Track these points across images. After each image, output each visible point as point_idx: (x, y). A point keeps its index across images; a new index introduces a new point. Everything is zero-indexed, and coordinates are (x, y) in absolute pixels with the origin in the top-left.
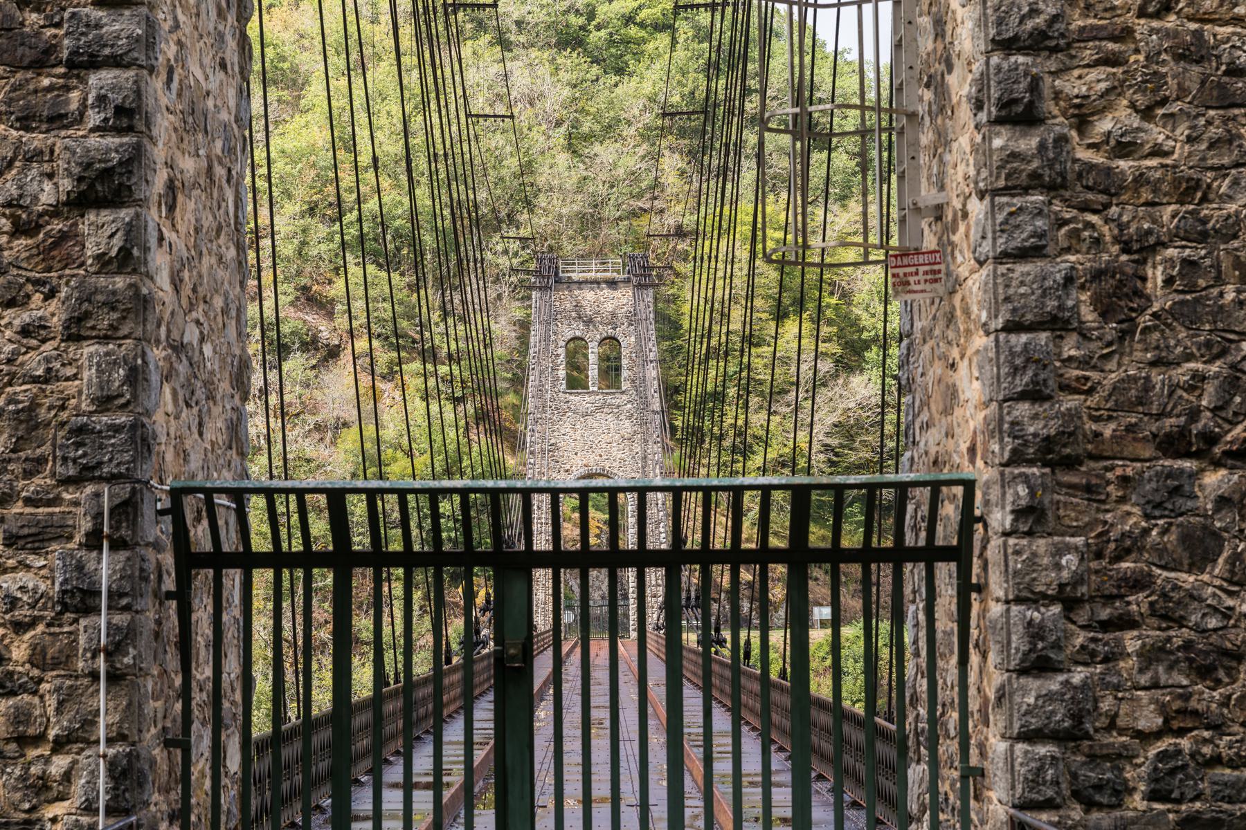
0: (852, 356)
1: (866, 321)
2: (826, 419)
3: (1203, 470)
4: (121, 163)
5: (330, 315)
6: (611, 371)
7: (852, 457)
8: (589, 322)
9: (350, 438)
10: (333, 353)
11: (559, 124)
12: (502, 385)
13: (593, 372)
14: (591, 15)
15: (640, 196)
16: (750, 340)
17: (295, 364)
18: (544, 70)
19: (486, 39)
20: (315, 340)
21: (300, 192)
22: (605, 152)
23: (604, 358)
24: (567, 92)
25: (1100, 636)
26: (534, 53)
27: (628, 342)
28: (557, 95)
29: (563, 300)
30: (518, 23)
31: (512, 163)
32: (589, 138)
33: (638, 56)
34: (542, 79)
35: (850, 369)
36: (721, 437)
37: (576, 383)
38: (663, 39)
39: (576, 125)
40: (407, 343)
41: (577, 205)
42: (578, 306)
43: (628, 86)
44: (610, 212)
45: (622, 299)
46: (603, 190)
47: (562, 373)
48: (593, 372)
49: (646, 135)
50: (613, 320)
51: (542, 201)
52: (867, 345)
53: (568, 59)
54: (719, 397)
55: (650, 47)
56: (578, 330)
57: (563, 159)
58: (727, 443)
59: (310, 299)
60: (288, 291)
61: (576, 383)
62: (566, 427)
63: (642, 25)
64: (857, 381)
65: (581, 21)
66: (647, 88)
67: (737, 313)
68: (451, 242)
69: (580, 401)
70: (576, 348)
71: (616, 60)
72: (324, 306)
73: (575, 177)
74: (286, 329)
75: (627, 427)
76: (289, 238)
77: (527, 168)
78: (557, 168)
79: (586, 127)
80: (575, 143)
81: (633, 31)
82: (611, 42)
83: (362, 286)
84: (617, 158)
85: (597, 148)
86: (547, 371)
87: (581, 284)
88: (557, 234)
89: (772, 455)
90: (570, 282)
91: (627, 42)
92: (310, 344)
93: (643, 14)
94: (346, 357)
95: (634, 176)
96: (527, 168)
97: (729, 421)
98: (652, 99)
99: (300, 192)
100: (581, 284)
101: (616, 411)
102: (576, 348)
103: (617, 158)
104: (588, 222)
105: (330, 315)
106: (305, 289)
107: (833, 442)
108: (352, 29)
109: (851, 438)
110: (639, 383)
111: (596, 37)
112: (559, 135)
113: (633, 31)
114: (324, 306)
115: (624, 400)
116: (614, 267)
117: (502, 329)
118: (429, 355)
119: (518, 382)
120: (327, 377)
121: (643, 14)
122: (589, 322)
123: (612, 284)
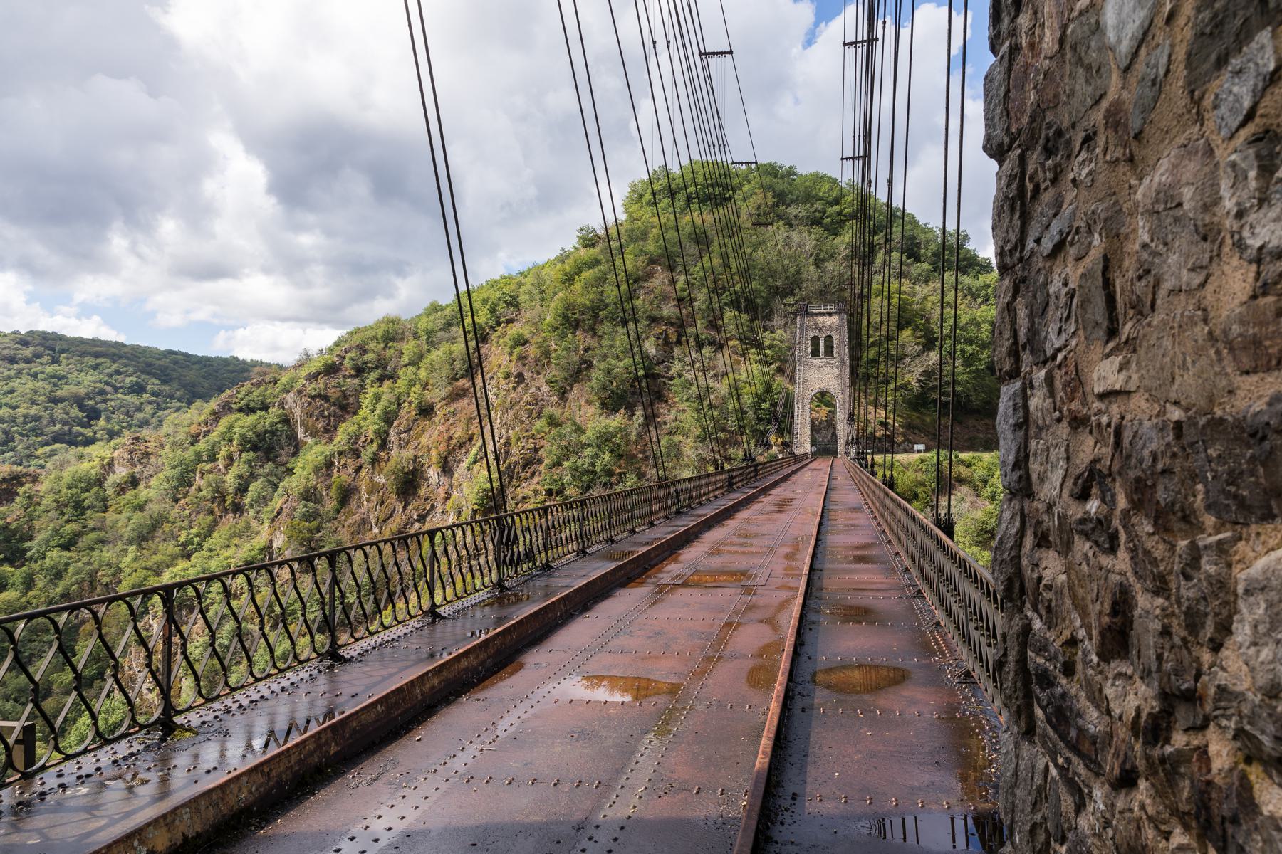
0: (929, 344)
3: (196, 756)
4: (1088, 539)
6: (829, 352)
8: (820, 330)
10: (721, 347)
13: (822, 350)
14: (824, 212)
16: (889, 338)
17: (706, 351)
18: (805, 235)
19: (782, 223)
22: (830, 266)
23: (826, 347)
25: (379, 407)
27: (836, 338)
28: (809, 243)
29: (809, 321)
32: (824, 260)
35: (929, 350)
36: (877, 378)
37: (815, 354)
39: (818, 255)
42: (816, 323)
45: (834, 320)
48: (822, 350)
50: (830, 329)
51: (804, 285)
54: (876, 361)
56: (816, 333)
57: (812, 268)
61: (815, 354)
67: (884, 327)
69: (817, 362)
70: (815, 340)
71: (834, 230)
77: (798, 272)
78: (811, 271)
79: (822, 255)
80: (818, 263)
82: (832, 223)
87: (817, 314)
96: (798, 272)
100: (817, 314)
102: (815, 340)
112: (811, 260)
115: (835, 361)
122: (820, 330)
123: (830, 314)
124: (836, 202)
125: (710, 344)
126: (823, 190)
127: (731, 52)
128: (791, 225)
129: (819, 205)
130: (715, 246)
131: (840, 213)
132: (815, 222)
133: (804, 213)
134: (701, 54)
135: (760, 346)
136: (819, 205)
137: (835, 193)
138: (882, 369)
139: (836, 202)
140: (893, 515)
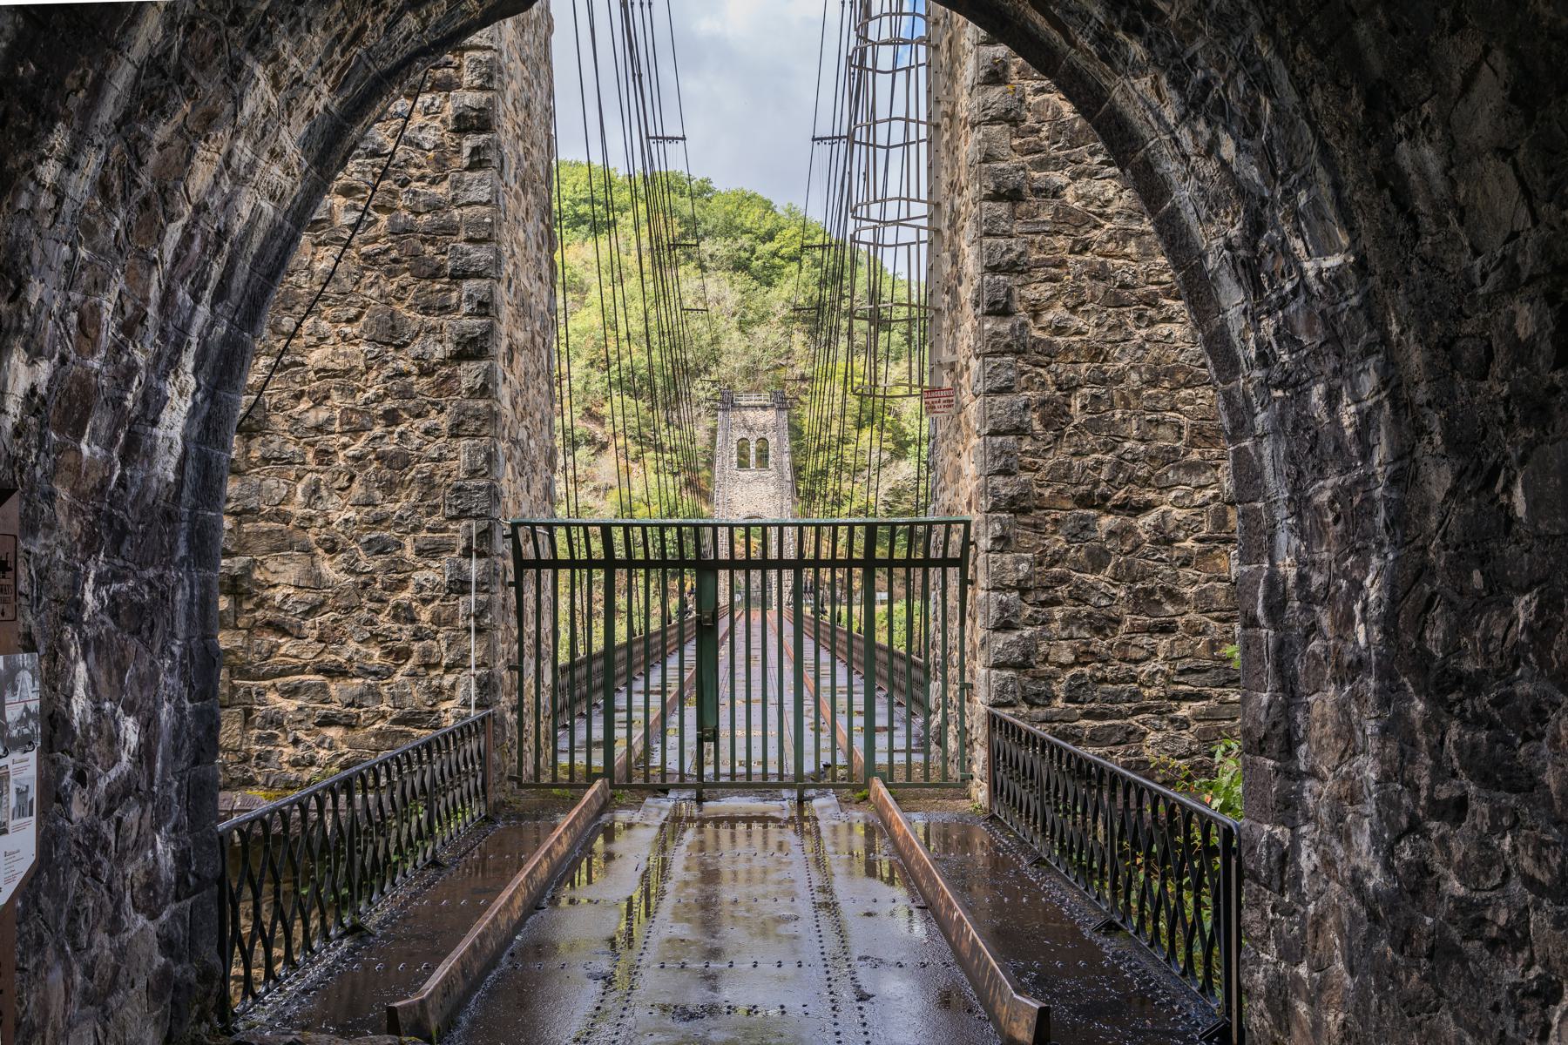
0: (900, 450)
1: (909, 430)
2: (885, 486)
5: (602, 425)
6: (763, 458)
7: (900, 508)
8: (751, 429)
9: (613, 496)
10: (604, 447)
11: (734, 315)
12: (701, 465)
13: (753, 458)
14: (753, 252)
15: (780, 357)
16: (843, 441)
17: (583, 452)
18: (726, 283)
20: (594, 439)
21: (585, 353)
22: (760, 331)
23: (759, 450)
24: (739, 296)
26: (720, 273)
27: (773, 441)
28: (732, 298)
29: (735, 417)
30: (711, 256)
31: (707, 338)
33: (780, 276)
34: (724, 290)
35: (899, 458)
37: (743, 465)
38: (794, 266)
40: (646, 441)
41: (745, 362)
42: (744, 420)
43: (774, 293)
44: (763, 366)
45: (769, 417)
46: (759, 353)
47: (735, 459)
48: (753, 458)
49: (785, 321)
50: (764, 428)
51: (724, 359)
52: (909, 444)
53: (740, 277)
54: (824, 473)
55: (787, 270)
57: (736, 335)
58: (829, 499)
59: (590, 415)
60: (578, 409)
61: (743, 465)
62: (737, 490)
63: (782, 258)
64: (903, 464)
65: (747, 255)
66: (785, 295)
68: (672, 383)
70: (743, 445)
71: (767, 278)
72: (599, 420)
73: (743, 346)
74: (577, 432)
75: (772, 489)
76: (578, 380)
77: (716, 340)
78: (733, 340)
80: (743, 326)
81: (777, 261)
82: (764, 268)
83: (622, 409)
84: (769, 334)
85: (756, 329)
86: (726, 458)
88: (732, 379)
89: (854, 506)
90: (740, 406)
91: (773, 267)
92: (591, 441)
93: (783, 251)
94: (612, 448)
95: (777, 345)
96: (716, 340)
97: (830, 486)
98: (788, 301)
99: (585, 353)
101: (765, 480)
103: (769, 334)
104: (750, 372)
105: (602, 425)
106: (588, 409)
107: (889, 499)
108: (615, 258)
109: (899, 497)
110: (779, 465)
111: (756, 264)
112: (734, 321)
113: (777, 261)
114: (599, 420)
116: (765, 399)
117: (701, 433)
118: (659, 448)
119: (710, 464)
120: (600, 460)
121: (783, 251)
122: (751, 429)
123: (764, 408)
124: (770, 236)
125: (588, 443)
126: (750, 217)
127: (684, 139)
128: (703, 268)
129: (745, 240)
130: (594, 295)
131: (775, 254)
132: (741, 266)
133: (724, 252)
134: (648, 138)
135: (659, 448)
136: (745, 240)
137: (768, 224)
138: (831, 483)
139: (770, 236)
140: (346, 77)
